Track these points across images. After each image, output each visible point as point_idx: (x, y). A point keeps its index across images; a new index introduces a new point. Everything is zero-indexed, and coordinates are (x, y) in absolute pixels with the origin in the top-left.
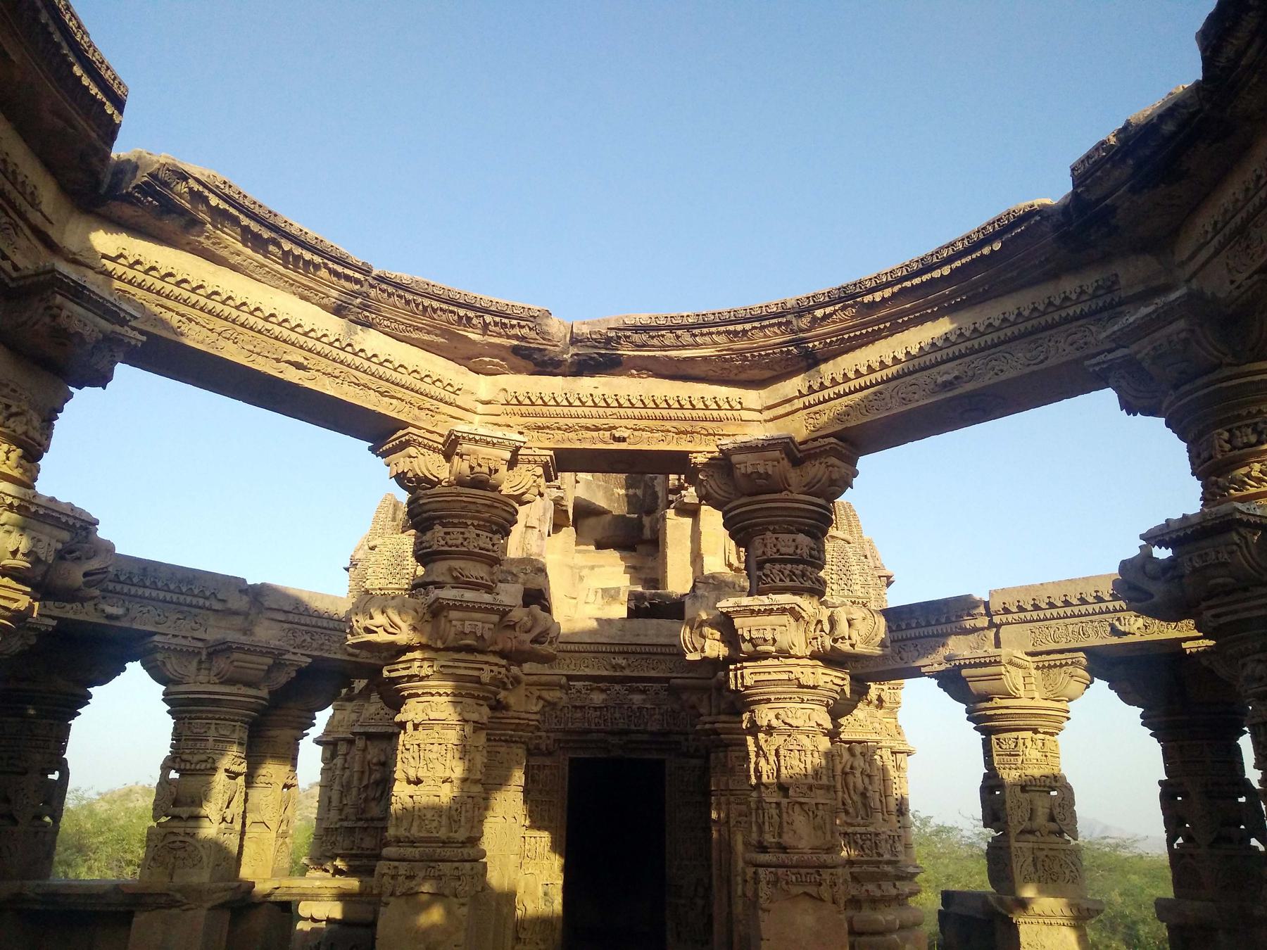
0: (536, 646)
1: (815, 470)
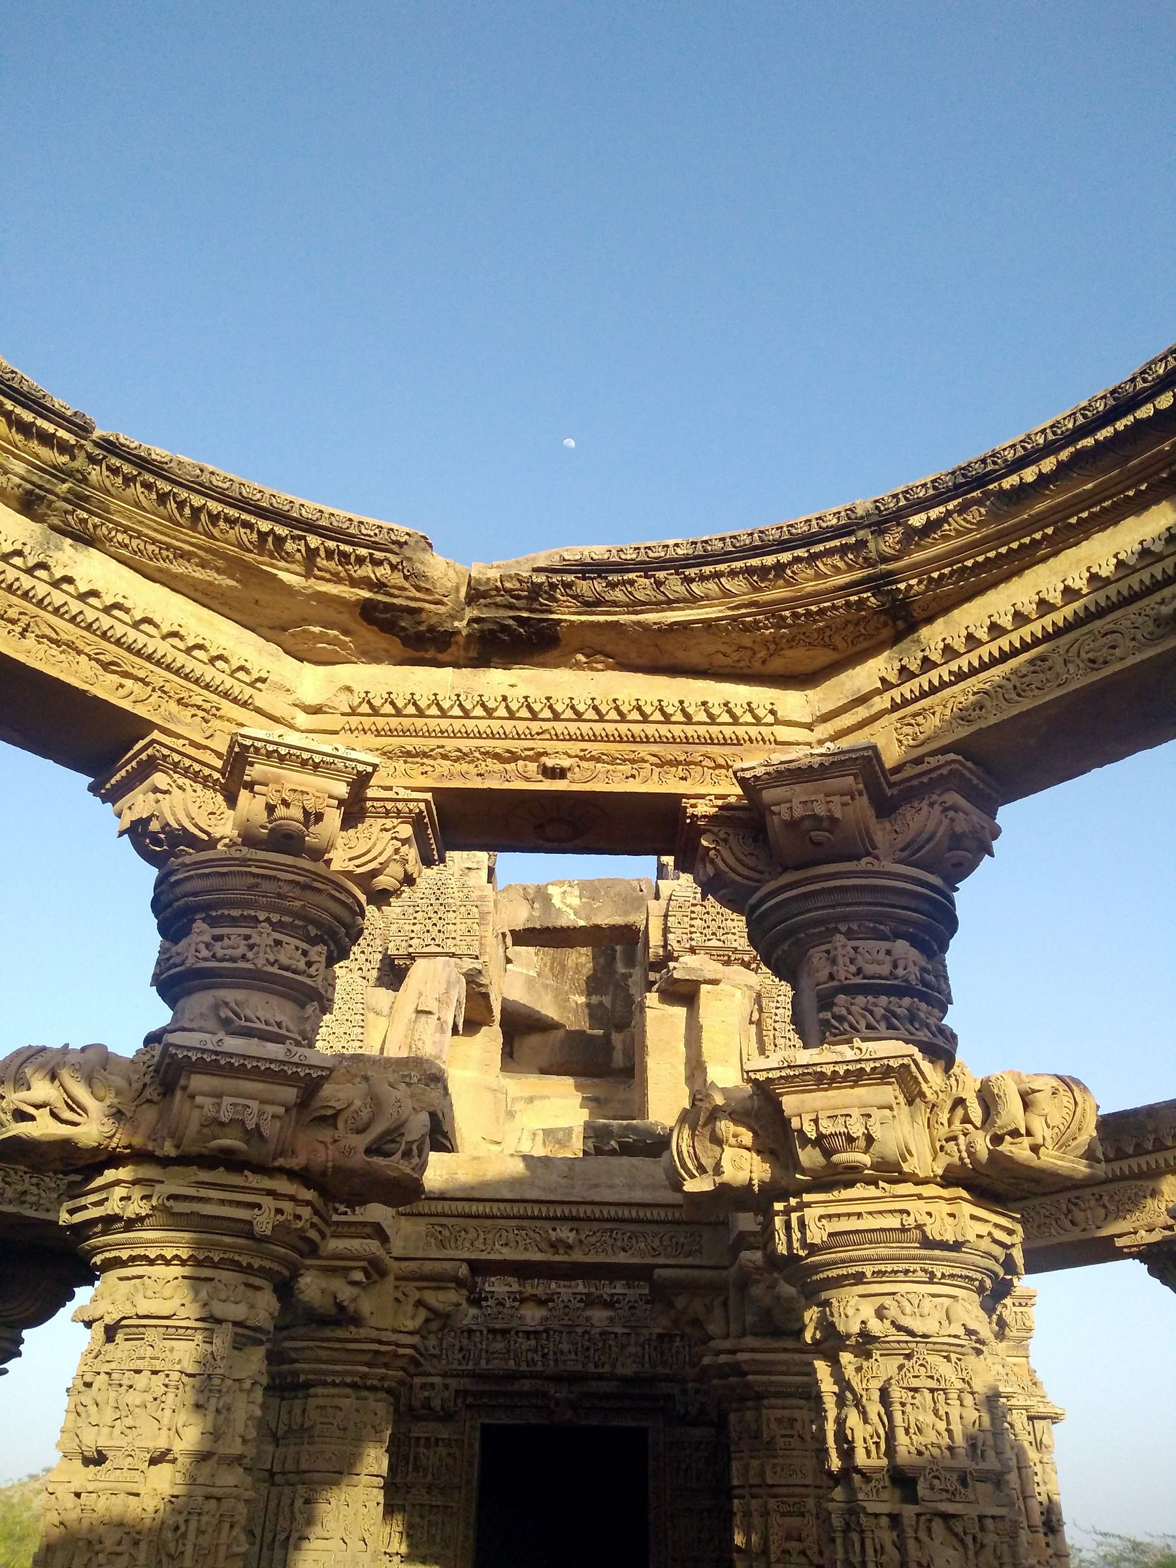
0: (379, 1161)
1: (923, 819)
